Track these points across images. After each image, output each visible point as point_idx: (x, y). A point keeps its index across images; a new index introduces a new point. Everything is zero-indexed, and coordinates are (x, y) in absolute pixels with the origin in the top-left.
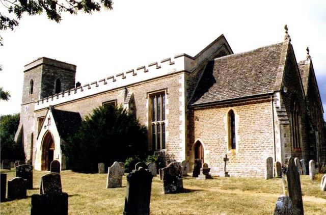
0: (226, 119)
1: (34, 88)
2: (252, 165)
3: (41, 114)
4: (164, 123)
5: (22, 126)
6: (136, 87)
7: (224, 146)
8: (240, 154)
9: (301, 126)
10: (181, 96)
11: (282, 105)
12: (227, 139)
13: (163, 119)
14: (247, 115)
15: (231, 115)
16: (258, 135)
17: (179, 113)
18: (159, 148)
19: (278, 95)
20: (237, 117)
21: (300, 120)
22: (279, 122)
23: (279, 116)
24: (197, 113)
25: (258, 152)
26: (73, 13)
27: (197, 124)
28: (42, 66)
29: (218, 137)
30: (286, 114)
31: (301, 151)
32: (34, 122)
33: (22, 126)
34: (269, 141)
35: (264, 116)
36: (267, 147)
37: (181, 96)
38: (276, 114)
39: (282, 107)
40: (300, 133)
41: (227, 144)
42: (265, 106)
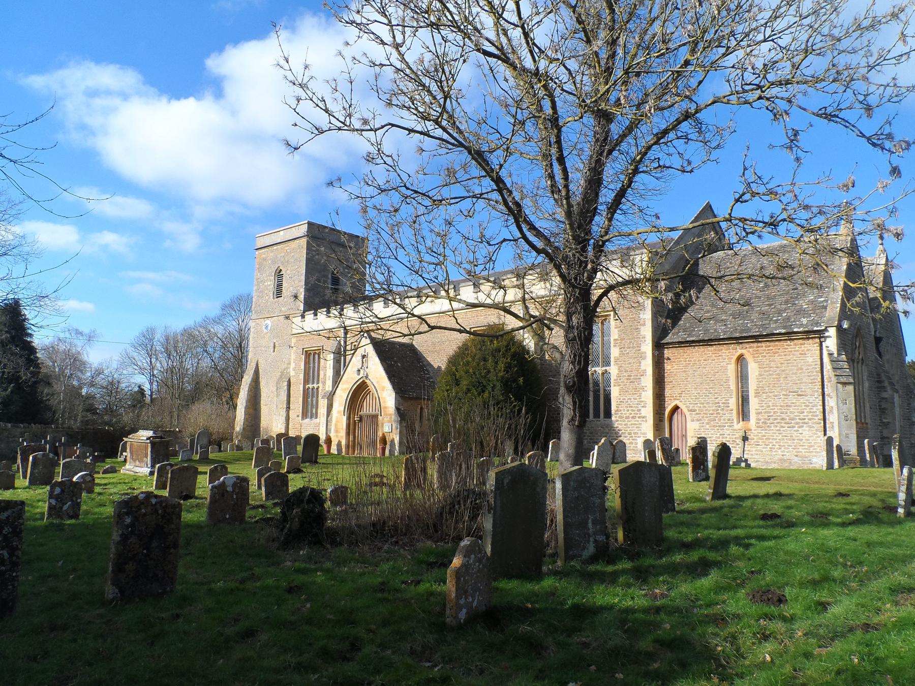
0: (731, 368)
1: (285, 285)
2: (783, 449)
3: (312, 343)
4: (606, 371)
5: (257, 365)
6: (782, 343)
7: (728, 416)
8: (759, 430)
9: (866, 384)
10: (644, 325)
11: (838, 351)
12: (733, 402)
13: (608, 364)
14: (772, 364)
15: (740, 359)
16: (792, 399)
17: (643, 357)
18: (597, 415)
19: (832, 332)
20: (753, 369)
21: (866, 374)
22: (834, 379)
23: (834, 369)
24: (667, 353)
25: (793, 427)
26: (307, 63)
27: (668, 367)
28: (304, 241)
29: (717, 401)
30: (846, 365)
31: (867, 428)
32: (293, 357)
33: (257, 365)
34: (815, 410)
35: (805, 368)
36: (810, 419)
37: (644, 325)
38: (828, 366)
39: (839, 354)
40: (866, 396)
41: (735, 412)
42: (808, 350)
